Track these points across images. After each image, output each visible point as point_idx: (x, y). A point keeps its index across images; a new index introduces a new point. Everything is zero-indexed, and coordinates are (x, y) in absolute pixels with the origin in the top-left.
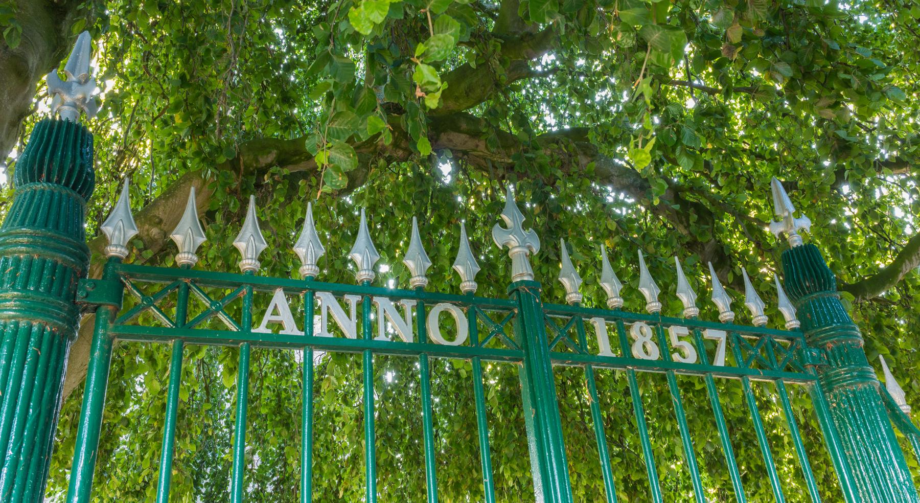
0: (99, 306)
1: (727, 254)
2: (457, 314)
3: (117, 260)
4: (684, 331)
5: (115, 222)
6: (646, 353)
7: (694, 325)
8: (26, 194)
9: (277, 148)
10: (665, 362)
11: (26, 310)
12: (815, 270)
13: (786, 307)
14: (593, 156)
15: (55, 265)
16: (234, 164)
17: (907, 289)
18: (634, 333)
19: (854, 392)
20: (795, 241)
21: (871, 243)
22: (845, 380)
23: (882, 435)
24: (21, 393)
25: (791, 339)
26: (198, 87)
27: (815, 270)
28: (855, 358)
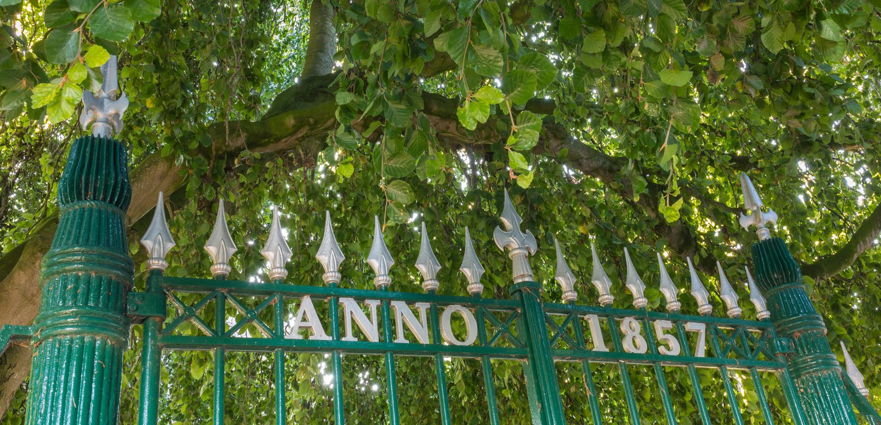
0: (147, 317)
1: (693, 236)
2: (467, 315)
3: (158, 272)
4: (669, 325)
5: (154, 235)
6: (636, 346)
7: (677, 318)
8: (75, 212)
9: (247, 131)
10: (653, 355)
11: (90, 326)
12: (782, 263)
13: (758, 298)
14: (563, 139)
15: (110, 281)
16: (203, 151)
17: (861, 266)
18: (624, 328)
19: (819, 378)
20: (764, 234)
21: (826, 221)
22: (811, 367)
23: (845, 418)
24: (92, 405)
25: (763, 329)
26: (173, 72)
27: (782, 263)
28: (819, 346)
